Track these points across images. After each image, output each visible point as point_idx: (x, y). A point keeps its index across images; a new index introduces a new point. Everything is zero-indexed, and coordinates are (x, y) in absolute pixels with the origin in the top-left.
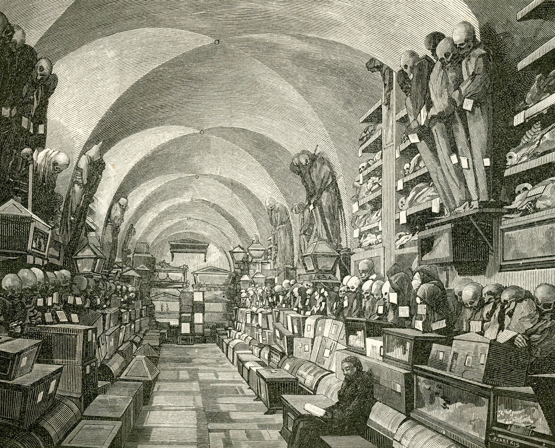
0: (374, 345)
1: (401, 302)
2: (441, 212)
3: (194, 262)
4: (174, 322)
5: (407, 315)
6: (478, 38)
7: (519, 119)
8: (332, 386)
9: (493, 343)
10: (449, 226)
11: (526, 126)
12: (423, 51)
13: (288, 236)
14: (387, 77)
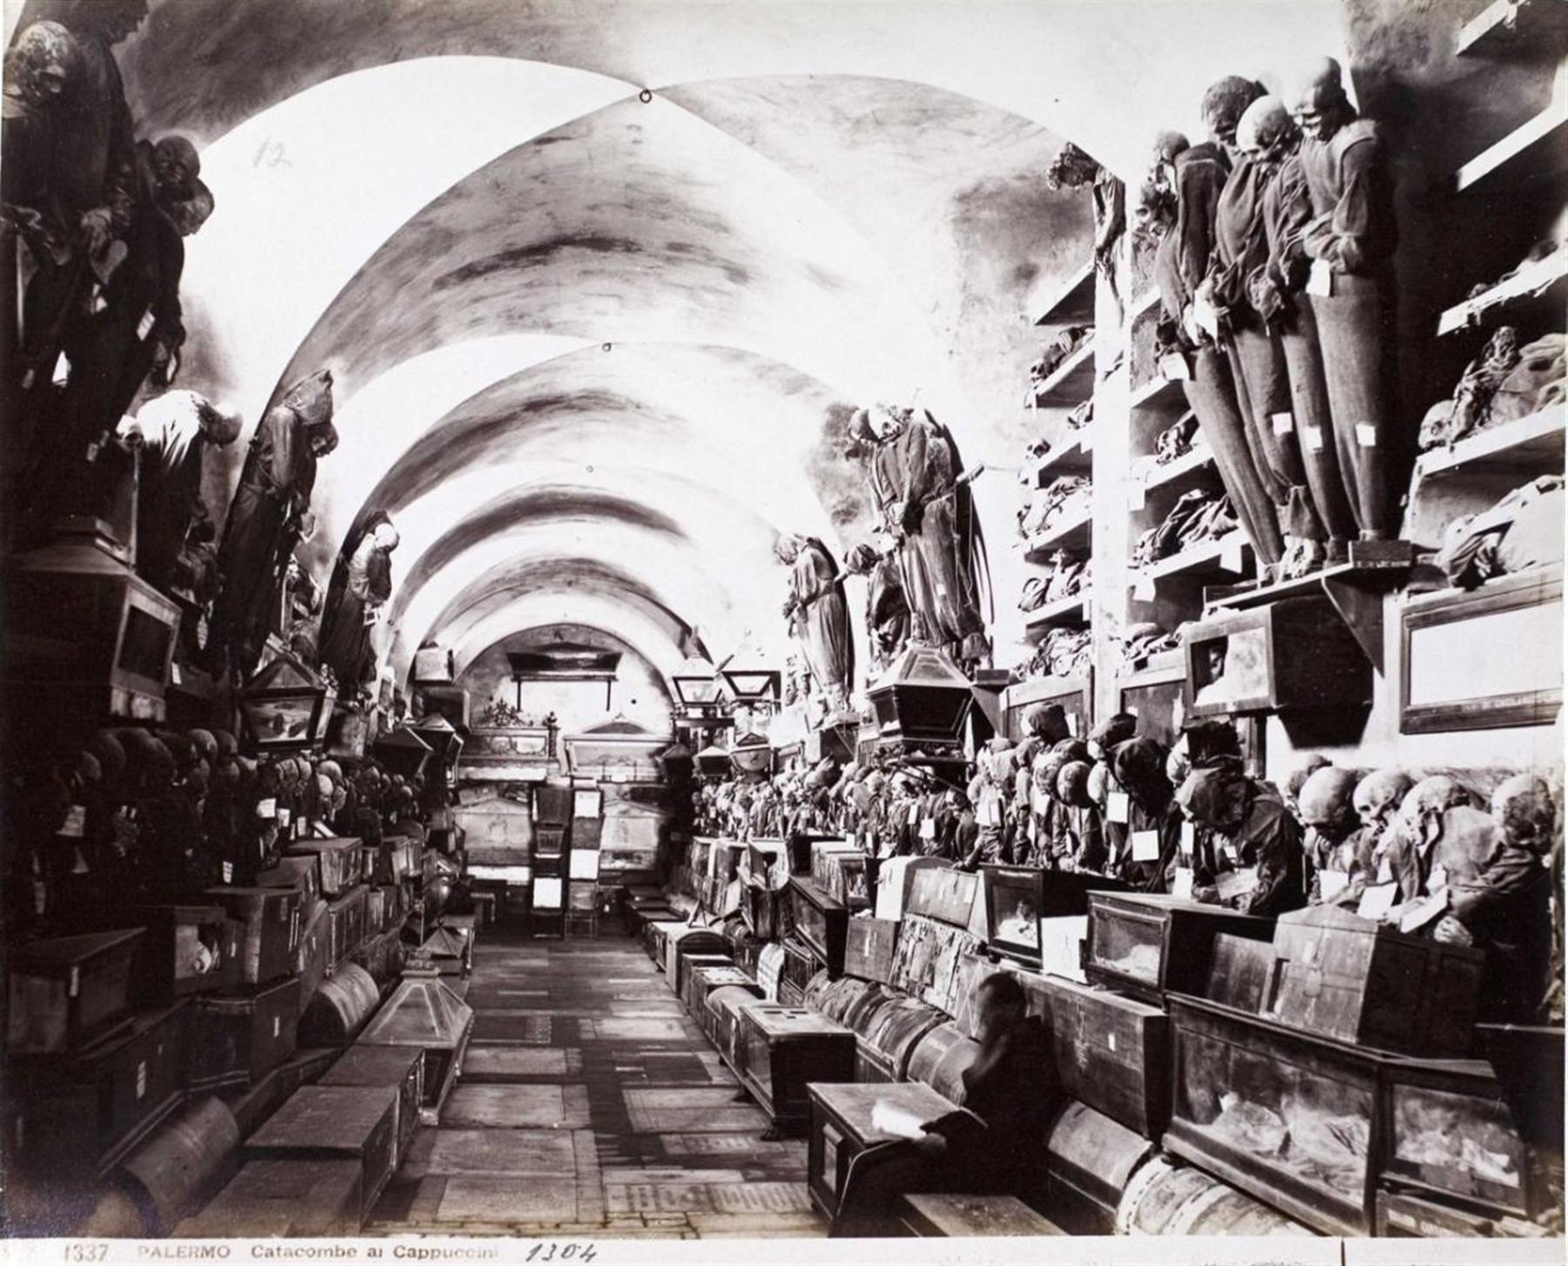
0: (1062, 937)
1: (1533, 1161)
2: (1249, 570)
3: (568, 702)
4: (518, 875)
5: (1153, 854)
6: (1352, 99)
7: (1453, 320)
8: (954, 1050)
9: (1388, 935)
10: (1265, 611)
11: (1473, 340)
12: (1201, 132)
13: (644, 997)
14: (1109, 203)
